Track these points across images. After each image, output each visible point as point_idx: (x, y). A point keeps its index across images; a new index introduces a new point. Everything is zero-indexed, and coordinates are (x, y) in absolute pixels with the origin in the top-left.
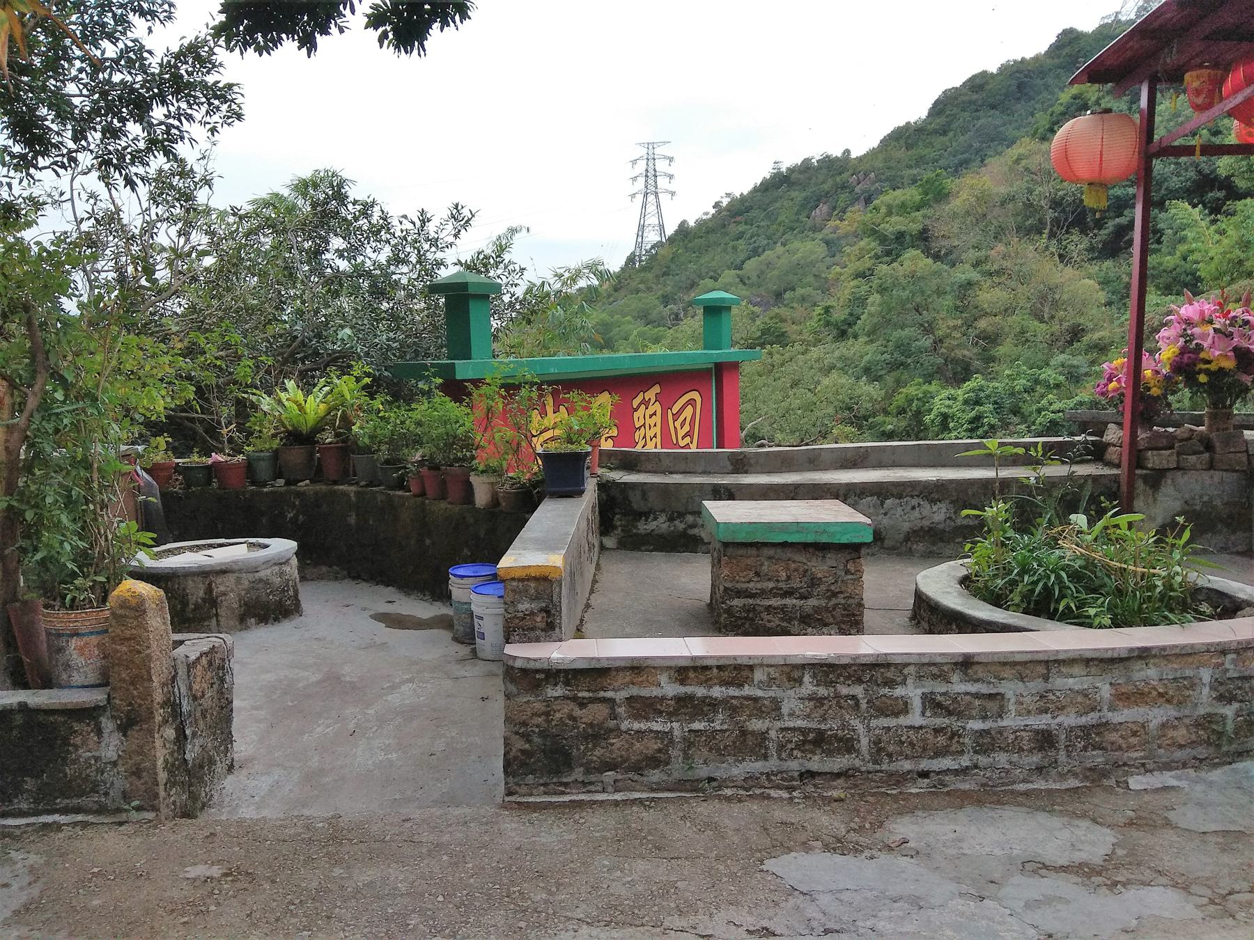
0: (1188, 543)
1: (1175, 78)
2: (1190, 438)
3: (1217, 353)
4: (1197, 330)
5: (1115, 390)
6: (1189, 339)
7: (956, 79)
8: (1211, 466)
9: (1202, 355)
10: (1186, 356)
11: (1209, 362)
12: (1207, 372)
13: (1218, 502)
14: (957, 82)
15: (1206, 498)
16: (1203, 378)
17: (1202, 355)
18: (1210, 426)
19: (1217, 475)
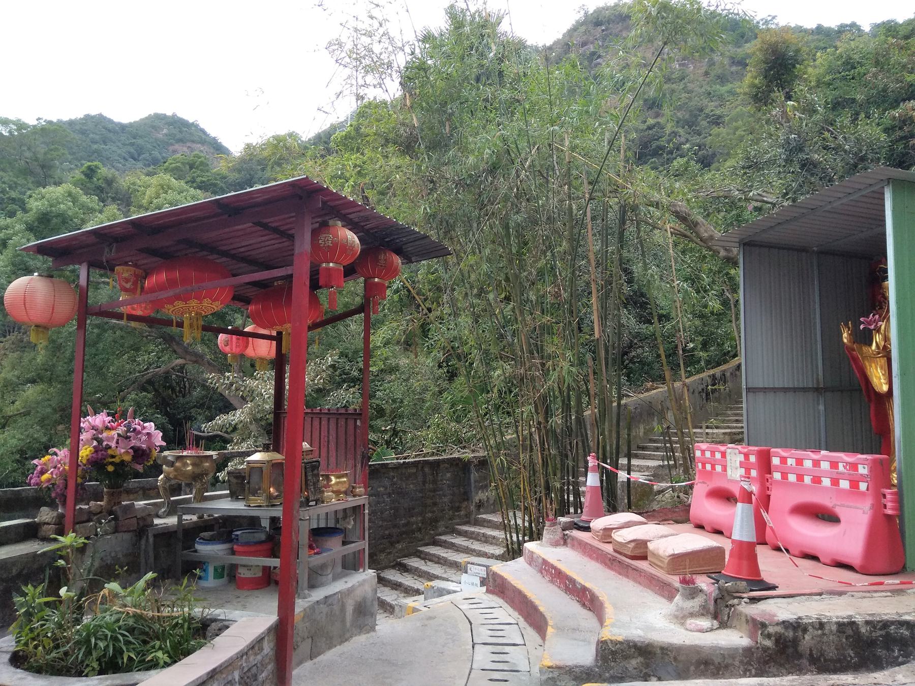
0: (186, 587)
1: (108, 267)
2: (101, 512)
3: (123, 451)
4: (105, 435)
5: (49, 480)
6: (100, 441)
7: (94, 112)
8: (116, 531)
9: (110, 452)
10: (100, 453)
11: (113, 457)
12: (112, 463)
13: (120, 555)
14: (65, 118)
15: (113, 554)
16: (110, 468)
17: (110, 452)
18: (109, 502)
19: (119, 535)
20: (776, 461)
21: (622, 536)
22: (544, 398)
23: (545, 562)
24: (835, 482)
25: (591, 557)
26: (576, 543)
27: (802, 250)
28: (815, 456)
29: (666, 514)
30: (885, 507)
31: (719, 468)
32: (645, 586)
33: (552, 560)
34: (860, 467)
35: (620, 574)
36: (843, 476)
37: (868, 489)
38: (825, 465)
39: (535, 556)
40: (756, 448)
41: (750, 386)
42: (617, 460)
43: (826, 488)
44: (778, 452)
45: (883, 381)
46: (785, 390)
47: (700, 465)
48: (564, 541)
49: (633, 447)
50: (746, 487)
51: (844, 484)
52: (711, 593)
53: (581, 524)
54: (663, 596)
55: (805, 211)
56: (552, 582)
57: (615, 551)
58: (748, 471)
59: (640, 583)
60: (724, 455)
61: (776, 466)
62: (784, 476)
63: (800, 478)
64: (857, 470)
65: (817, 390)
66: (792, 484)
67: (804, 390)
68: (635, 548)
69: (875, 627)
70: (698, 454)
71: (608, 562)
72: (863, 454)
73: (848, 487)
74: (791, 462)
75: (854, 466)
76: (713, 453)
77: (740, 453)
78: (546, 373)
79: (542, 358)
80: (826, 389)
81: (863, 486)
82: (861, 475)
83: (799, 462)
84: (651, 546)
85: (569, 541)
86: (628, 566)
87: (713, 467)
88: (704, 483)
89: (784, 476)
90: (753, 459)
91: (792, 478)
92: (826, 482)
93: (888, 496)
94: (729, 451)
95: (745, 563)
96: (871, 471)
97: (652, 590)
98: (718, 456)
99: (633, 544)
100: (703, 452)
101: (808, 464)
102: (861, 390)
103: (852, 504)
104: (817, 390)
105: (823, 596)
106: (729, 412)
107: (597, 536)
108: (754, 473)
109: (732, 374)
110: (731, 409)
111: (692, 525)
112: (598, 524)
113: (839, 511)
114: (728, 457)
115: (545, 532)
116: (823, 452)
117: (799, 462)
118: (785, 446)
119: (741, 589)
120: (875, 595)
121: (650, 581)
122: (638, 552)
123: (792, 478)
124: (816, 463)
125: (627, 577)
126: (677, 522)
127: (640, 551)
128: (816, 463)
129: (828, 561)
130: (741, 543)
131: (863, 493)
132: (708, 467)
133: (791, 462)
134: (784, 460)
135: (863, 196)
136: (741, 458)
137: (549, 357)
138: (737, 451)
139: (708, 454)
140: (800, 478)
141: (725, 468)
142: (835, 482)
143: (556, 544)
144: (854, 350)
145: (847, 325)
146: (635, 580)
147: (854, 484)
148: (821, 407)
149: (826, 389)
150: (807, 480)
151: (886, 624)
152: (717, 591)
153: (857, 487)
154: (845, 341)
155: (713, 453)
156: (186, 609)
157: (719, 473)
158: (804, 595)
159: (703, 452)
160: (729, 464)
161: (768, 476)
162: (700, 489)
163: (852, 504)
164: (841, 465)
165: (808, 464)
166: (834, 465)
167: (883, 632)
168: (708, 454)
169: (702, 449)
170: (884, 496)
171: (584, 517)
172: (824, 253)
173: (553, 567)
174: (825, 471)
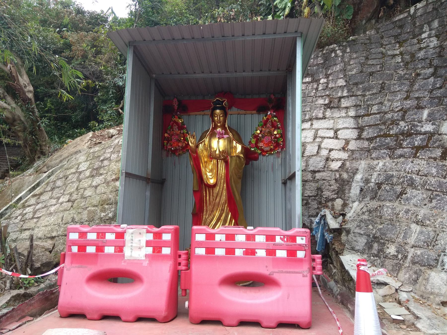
24: (271, 252)
30: (180, 264)
37: (305, 257)
43: (261, 258)
51: (281, 254)
58: (157, 249)
60: (120, 236)
73: (286, 256)
77: (148, 232)
81: (301, 254)
82: (300, 245)
92: (261, 253)
101: (241, 238)
103: (296, 270)
108: (166, 251)
113: (276, 276)
114: (127, 237)
124: (250, 237)
126: (35, 316)
129: (273, 324)
131: (301, 260)
136: (150, 237)
141: (120, 249)
147: (292, 253)
148: (148, 194)
165: (241, 238)
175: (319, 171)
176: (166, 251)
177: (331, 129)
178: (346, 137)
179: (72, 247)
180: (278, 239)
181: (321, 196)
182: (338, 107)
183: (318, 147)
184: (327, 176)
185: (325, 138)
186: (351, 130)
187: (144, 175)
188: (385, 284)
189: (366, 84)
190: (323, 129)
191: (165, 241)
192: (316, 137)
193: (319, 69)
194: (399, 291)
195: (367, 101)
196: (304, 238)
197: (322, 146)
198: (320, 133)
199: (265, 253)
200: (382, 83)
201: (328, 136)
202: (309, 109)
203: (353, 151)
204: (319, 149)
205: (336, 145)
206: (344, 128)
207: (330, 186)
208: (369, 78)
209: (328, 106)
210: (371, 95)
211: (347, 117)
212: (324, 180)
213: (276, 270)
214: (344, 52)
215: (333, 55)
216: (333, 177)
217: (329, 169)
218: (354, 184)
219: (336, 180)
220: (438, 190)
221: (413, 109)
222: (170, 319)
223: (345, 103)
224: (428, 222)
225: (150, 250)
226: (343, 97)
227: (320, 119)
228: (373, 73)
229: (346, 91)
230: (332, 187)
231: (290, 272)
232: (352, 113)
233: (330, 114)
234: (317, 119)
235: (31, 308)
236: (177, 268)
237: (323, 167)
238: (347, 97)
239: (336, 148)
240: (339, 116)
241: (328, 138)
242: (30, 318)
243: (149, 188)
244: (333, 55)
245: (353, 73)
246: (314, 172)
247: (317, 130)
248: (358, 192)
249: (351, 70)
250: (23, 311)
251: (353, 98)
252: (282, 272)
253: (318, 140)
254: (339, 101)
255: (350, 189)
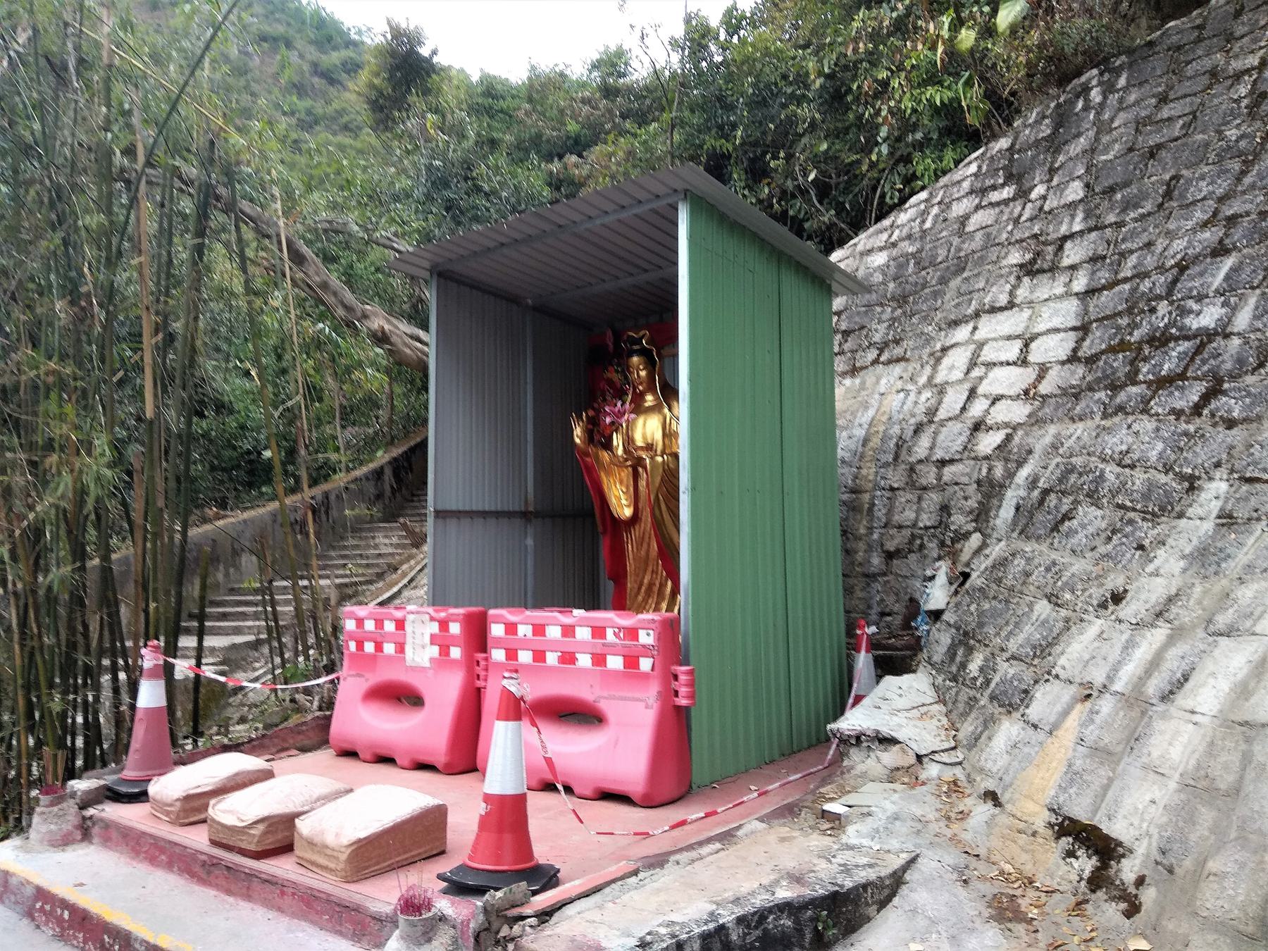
20: (497, 630)
21: (238, 810)
22: (37, 532)
23: (42, 894)
24: (599, 660)
25: (152, 861)
26: (114, 835)
27: (512, 299)
28: (567, 620)
29: (284, 740)
30: (676, 693)
31: (389, 648)
32: (294, 915)
33: (61, 887)
34: (642, 633)
35: (229, 892)
36: (525, 644)
37: (653, 669)
38: (583, 633)
39: (13, 881)
40: (461, 611)
41: (439, 508)
42: (176, 640)
43: (584, 671)
44: (502, 616)
45: (624, 502)
46: (484, 514)
47: (352, 646)
48: (85, 831)
49: (184, 615)
50: (513, 689)
51: (615, 662)
52: (465, 924)
53: (124, 789)
54: (340, 933)
55: (547, 227)
56: (61, 937)
57: (214, 843)
58: (445, 651)
59: (280, 909)
60: (400, 625)
61: (498, 639)
62: (512, 654)
63: (539, 656)
64: (636, 638)
65: (525, 515)
66: (526, 667)
67: (509, 515)
68: (265, 833)
69: (748, 927)
70: (350, 625)
71: (197, 869)
72: (456, 607)
73: (621, 667)
74: (524, 630)
75: (632, 633)
76: (379, 624)
77: (432, 619)
78: (42, 479)
79: (30, 447)
80: (537, 514)
81: (645, 664)
82: (644, 646)
83: (539, 630)
84: (304, 826)
85: (96, 830)
86: (252, 876)
87: (379, 647)
88: (359, 675)
89: (512, 654)
90: (455, 628)
91: (525, 657)
92: (584, 660)
93: (683, 678)
94: (410, 617)
95: (508, 837)
96: (658, 638)
97: (313, 922)
98: (389, 626)
99: (261, 827)
100: (360, 622)
101: (554, 632)
102: (593, 515)
104: (525, 515)
105: (641, 875)
106: (333, 554)
107: (168, 813)
108: (456, 653)
109: (337, 496)
110: (334, 548)
111: (331, 752)
112: (173, 785)
113: (605, 706)
114: (409, 627)
115: (36, 819)
116: (576, 612)
117: (539, 630)
118: (510, 604)
119: (519, 896)
120: (706, 850)
121: (308, 905)
122: (270, 843)
123: (525, 657)
124: (568, 631)
125: (248, 897)
126: (304, 750)
127: (280, 836)
128: (568, 631)
129: (588, 793)
130: (502, 798)
131: (645, 676)
132: (369, 647)
133: (524, 630)
134: (511, 628)
135: (619, 221)
136: (435, 628)
137: (49, 446)
138: (427, 617)
139: (370, 625)
140: (539, 656)
141: (401, 648)
142: (599, 660)
143: (64, 842)
144: (588, 455)
145: (580, 417)
146: (268, 904)
147: (631, 662)
148: (530, 542)
149: (537, 514)
150: (552, 658)
151: (761, 915)
152: (481, 917)
153: (637, 666)
154: (578, 441)
155: (379, 624)
156: (806, 112)
157: (389, 657)
158: (614, 881)
159: (360, 622)
160: (409, 640)
161: (480, 656)
162: (351, 686)
163: (630, 695)
164: (610, 632)
165: (554, 632)
166: (598, 632)
167: (758, 933)
168: (370, 625)
169: (356, 618)
170: (676, 677)
171: (129, 774)
172: (542, 310)
173: (65, 904)
174: (584, 643)
175: (952, 461)
176: (456, 653)
177: (1018, 337)
178: (1041, 361)
179: (452, 649)
180: (610, 635)
181: (947, 527)
182: (1053, 269)
183: (967, 393)
184: (963, 475)
185: (995, 364)
186: (1062, 335)
187: (516, 506)
188: (887, 741)
189: (1133, 189)
190: (995, 339)
191: (453, 636)
192: (975, 364)
193: (1039, 154)
194: (925, 760)
195: (1123, 240)
196: (651, 632)
197: (980, 390)
198: (988, 354)
199: (590, 661)
200: (1172, 178)
201: (1003, 359)
202: (981, 285)
203: (1045, 397)
204: (968, 398)
205: (1011, 385)
206: (1049, 331)
207: (966, 498)
208: (1146, 165)
209: (1029, 270)
210: (1136, 220)
211: (1068, 294)
212: (957, 484)
213: (605, 694)
214: (1109, 88)
215: (1080, 104)
216: (975, 476)
217: (973, 455)
218: (1010, 494)
219: (979, 482)
220: (1139, 507)
221: (1205, 257)
222: (461, 768)
223: (1073, 253)
224: (1068, 596)
225: (435, 650)
226: (1071, 236)
227: (1002, 309)
228: (1159, 146)
229: (1080, 216)
230: (970, 502)
231: (622, 699)
232: (1080, 284)
233: (1027, 294)
234: (993, 310)
235: (301, 737)
236: (473, 683)
237: (960, 449)
238: (1081, 233)
239: (1012, 393)
240: (1046, 296)
241: (1002, 364)
242: (294, 752)
243: (530, 530)
244: (1080, 104)
245: (1110, 157)
246: (943, 463)
247: (981, 345)
248: (1012, 511)
249: (1106, 150)
250: (284, 740)
251: (1094, 234)
252: (614, 698)
253: (977, 372)
254: (1061, 248)
255: (1000, 507)
